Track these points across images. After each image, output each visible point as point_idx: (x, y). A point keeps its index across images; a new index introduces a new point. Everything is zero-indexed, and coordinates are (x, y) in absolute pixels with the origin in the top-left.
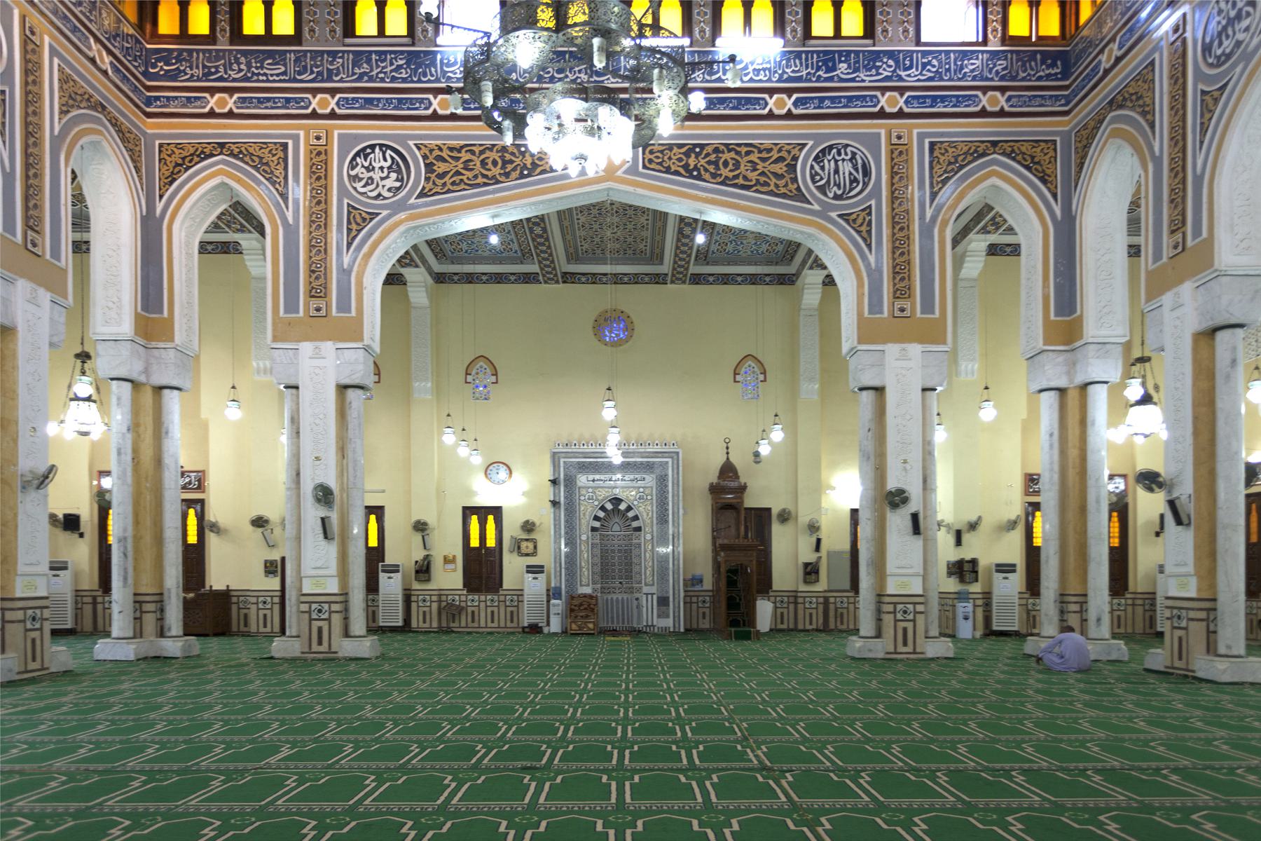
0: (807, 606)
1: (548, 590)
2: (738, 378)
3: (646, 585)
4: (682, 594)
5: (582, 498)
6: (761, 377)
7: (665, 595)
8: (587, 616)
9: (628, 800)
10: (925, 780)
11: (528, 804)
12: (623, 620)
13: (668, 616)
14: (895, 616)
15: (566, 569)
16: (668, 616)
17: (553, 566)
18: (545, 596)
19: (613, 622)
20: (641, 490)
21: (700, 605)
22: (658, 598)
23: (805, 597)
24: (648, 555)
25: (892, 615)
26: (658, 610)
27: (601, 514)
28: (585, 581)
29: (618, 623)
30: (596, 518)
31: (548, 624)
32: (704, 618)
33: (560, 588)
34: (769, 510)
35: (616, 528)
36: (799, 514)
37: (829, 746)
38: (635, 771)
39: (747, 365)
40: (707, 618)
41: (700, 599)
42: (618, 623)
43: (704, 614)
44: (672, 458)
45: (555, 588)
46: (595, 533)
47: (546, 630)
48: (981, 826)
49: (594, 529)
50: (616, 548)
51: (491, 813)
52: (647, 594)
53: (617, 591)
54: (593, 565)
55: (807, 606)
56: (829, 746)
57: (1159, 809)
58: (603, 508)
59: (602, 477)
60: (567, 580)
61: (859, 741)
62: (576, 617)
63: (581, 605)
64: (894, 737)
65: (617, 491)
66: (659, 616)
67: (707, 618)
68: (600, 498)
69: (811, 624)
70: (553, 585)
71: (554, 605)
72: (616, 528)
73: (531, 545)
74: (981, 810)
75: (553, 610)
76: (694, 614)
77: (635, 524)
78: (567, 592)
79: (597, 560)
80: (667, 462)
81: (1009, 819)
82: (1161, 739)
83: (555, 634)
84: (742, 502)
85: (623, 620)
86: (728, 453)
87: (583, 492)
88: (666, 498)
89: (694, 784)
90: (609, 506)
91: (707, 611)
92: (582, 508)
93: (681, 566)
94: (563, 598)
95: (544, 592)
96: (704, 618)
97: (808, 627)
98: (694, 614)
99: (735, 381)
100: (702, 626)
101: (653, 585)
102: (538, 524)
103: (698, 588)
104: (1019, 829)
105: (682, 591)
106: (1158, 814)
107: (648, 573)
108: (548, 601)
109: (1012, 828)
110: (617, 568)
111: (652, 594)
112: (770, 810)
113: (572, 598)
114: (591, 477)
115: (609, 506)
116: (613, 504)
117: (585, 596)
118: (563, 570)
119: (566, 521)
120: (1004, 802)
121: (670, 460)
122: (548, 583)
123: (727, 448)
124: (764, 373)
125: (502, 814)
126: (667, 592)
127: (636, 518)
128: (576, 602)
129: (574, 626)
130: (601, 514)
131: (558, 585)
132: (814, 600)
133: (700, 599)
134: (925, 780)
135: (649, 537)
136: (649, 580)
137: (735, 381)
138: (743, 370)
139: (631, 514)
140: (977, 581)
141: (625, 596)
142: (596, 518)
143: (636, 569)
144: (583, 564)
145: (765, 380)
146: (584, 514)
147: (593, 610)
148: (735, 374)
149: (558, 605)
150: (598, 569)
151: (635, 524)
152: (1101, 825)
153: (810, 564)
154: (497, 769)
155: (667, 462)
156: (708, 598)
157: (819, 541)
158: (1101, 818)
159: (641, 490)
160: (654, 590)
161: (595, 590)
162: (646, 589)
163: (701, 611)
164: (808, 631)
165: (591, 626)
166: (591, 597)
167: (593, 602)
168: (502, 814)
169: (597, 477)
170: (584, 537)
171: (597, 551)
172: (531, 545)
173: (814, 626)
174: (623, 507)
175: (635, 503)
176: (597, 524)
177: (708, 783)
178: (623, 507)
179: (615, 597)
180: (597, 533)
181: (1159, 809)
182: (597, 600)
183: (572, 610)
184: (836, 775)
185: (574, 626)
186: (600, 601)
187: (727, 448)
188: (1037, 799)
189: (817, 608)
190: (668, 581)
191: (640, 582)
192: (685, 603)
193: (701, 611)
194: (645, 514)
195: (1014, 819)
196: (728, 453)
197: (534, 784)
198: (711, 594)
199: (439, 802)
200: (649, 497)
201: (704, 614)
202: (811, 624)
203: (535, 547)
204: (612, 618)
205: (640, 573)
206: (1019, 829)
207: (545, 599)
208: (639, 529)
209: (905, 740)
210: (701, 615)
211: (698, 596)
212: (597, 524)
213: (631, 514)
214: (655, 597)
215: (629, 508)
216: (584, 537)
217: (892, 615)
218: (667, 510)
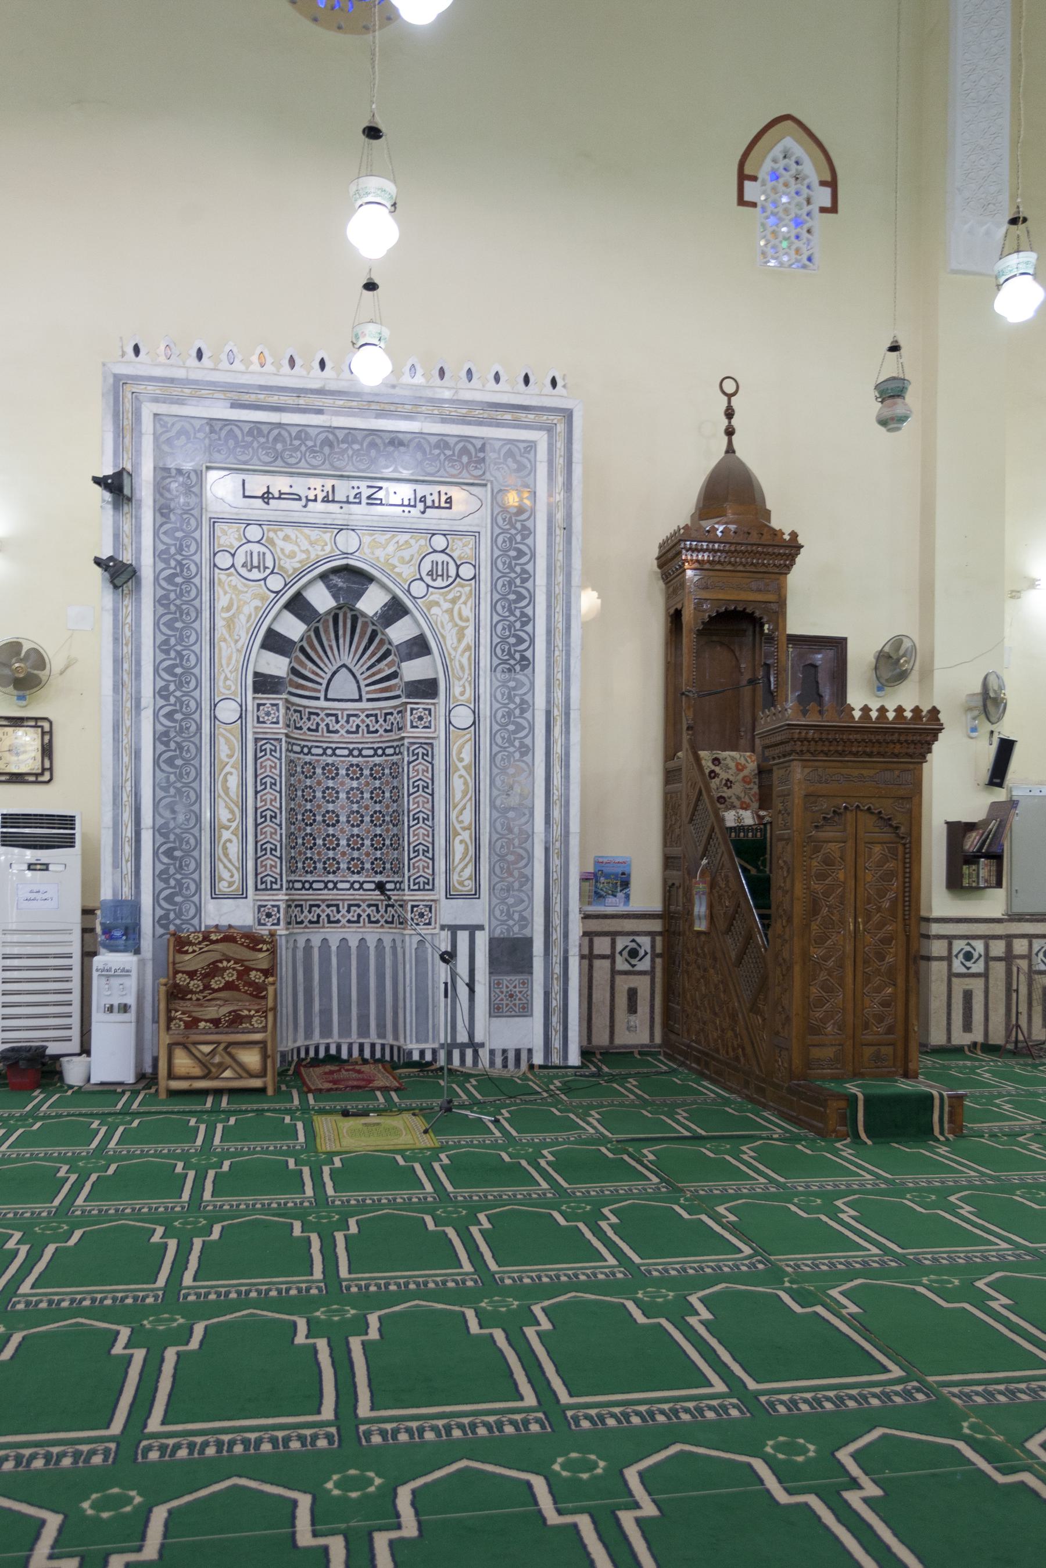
0: (958, 967)
1: (87, 912)
2: (751, 190)
3: (449, 896)
4: (576, 929)
5: (223, 560)
6: (823, 196)
7: (516, 932)
8: (236, 1020)
9: (330, 1191)
10: (662, 1117)
11: (202, 1147)
12: (363, 1018)
13: (525, 1010)
14: (950, 966)
15: (158, 830)
16: (525, 1010)
17: (108, 819)
18: (76, 937)
19: (326, 1031)
20: (439, 542)
21: (621, 965)
22: (493, 941)
23: (950, 939)
24: (458, 784)
25: (945, 964)
26: (493, 986)
27: (293, 628)
28: (228, 877)
29: (345, 1030)
30: (274, 642)
31: (85, 1050)
32: (632, 1009)
33: (135, 907)
34: (838, 645)
35: (344, 686)
36: (938, 663)
37: (593, 1113)
38: (368, 1301)
39: (777, 151)
40: (643, 1007)
41: (621, 943)
42: (345, 1030)
43: (632, 994)
44: (550, 429)
45: (118, 904)
46: (268, 699)
47: (74, 1072)
48: (805, 1215)
49: (264, 684)
50: (342, 761)
51: (98, 1312)
52: (454, 929)
53: (343, 916)
54: (261, 817)
55: (958, 967)
56: (593, 1113)
57: (1019, 1187)
58: (298, 605)
59: (300, 486)
60: (161, 876)
61: (632, 1105)
62: (193, 1023)
63: (214, 970)
64: (680, 1099)
65: (348, 542)
66: (496, 1010)
67: (643, 1007)
68: (290, 565)
69: (967, 1027)
70: (106, 894)
71: (108, 974)
72: (344, 686)
73: (28, 740)
74: (802, 1194)
75: (102, 994)
76: (601, 995)
77: (414, 670)
78: (161, 921)
79: (274, 799)
80: (531, 446)
81: (839, 1203)
82: (1009, 1094)
83: (109, 1090)
84: (778, 609)
85: (363, 1018)
86: (730, 432)
87: (228, 536)
88: (526, 576)
89: (417, 1167)
90: (322, 600)
91: (642, 984)
92: (222, 601)
93: (575, 827)
94: (147, 943)
95: (75, 920)
96: (632, 1009)
97: (961, 1038)
98: (601, 995)
99: (741, 201)
100: (624, 1038)
101: (476, 894)
102: (56, 661)
103: (613, 905)
104: (1003, 1306)
105: (575, 917)
106: (1018, 1192)
107: (458, 849)
108: (88, 955)
109: (841, 1215)
110: (343, 832)
111: (473, 929)
112: (528, 1201)
113: (181, 944)
114: (257, 484)
115: (322, 600)
116: (335, 593)
117: (229, 936)
118: (147, 837)
119: (163, 647)
120: (829, 1183)
121: (540, 438)
122: (90, 883)
123: (729, 414)
124: (832, 184)
125: (118, 1313)
126: (526, 921)
127: (419, 647)
128: (192, 961)
129: (183, 1062)
130: (293, 628)
131: (127, 893)
132: (979, 946)
133: (621, 943)
134: (662, 1117)
135: (462, 717)
136: (463, 875)
137: (741, 201)
138: (767, 166)
139: (399, 633)
140: (999, 884)
141: (372, 935)
142: (274, 642)
143: (415, 835)
144: (223, 815)
145: (833, 209)
146: (230, 624)
147: (258, 992)
148: (743, 177)
149: (125, 973)
150: (276, 834)
151: (414, 670)
152: (953, 1209)
153: (970, 827)
154: (55, 1313)
155: (531, 446)
156: (645, 942)
157: (1006, 748)
158: (952, 1199)
159: (439, 542)
160: (476, 912)
161: (265, 913)
162: (449, 912)
163: (623, 984)
164: (958, 1050)
165: (251, 1058)
166: (253, 941)
167: (261, 959)
168: (118, 1313)
169: (280, 484)
170: (228, 712)
171: (275, 767)
172: (28, 740)
173: (977, 1036)
174: (371, 603)
175: (418, 589)
176: (277, 665)
177: (436, 1166)
178: (371, 603)
179: (334, 936)
180: (280, 699)
181: (1019, 1187)
182: (273, 952)
183: (176, 994)
184: (558, 1110)
185: (183, 1062)
186: (284, 954)
187: (729, 414)
188: (869, 1177)
189: (985, 975)
190: (529, 879)
191: (429, 885)
192: (589, 958)
193: (623, 984)
194: (451, 640)
195: (844, 1203)
196: (730, 432)
197: (172, 1244)
198: (656, 926)
199: (57, 1202)
200: (467, 572)
201: (632, 994)
202: (967, 1027)
203: (47, 751)
204: (326, 1012)
205: (429, 851)
206: (1003, 1306)
207: (76, 950)
208: (427, 688)
209: (695, 1102)
210: (622, 1001)
211: (613, 935)
212: (277, 665)
213: (399, 633)
214: (482, 939)
215: (395, 610)
216: (228, 712)
217: (945, 964)
218: (527, 620)
